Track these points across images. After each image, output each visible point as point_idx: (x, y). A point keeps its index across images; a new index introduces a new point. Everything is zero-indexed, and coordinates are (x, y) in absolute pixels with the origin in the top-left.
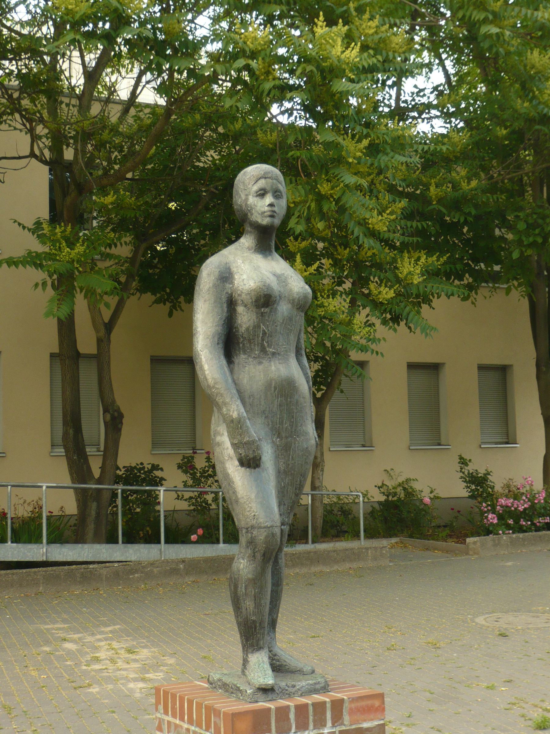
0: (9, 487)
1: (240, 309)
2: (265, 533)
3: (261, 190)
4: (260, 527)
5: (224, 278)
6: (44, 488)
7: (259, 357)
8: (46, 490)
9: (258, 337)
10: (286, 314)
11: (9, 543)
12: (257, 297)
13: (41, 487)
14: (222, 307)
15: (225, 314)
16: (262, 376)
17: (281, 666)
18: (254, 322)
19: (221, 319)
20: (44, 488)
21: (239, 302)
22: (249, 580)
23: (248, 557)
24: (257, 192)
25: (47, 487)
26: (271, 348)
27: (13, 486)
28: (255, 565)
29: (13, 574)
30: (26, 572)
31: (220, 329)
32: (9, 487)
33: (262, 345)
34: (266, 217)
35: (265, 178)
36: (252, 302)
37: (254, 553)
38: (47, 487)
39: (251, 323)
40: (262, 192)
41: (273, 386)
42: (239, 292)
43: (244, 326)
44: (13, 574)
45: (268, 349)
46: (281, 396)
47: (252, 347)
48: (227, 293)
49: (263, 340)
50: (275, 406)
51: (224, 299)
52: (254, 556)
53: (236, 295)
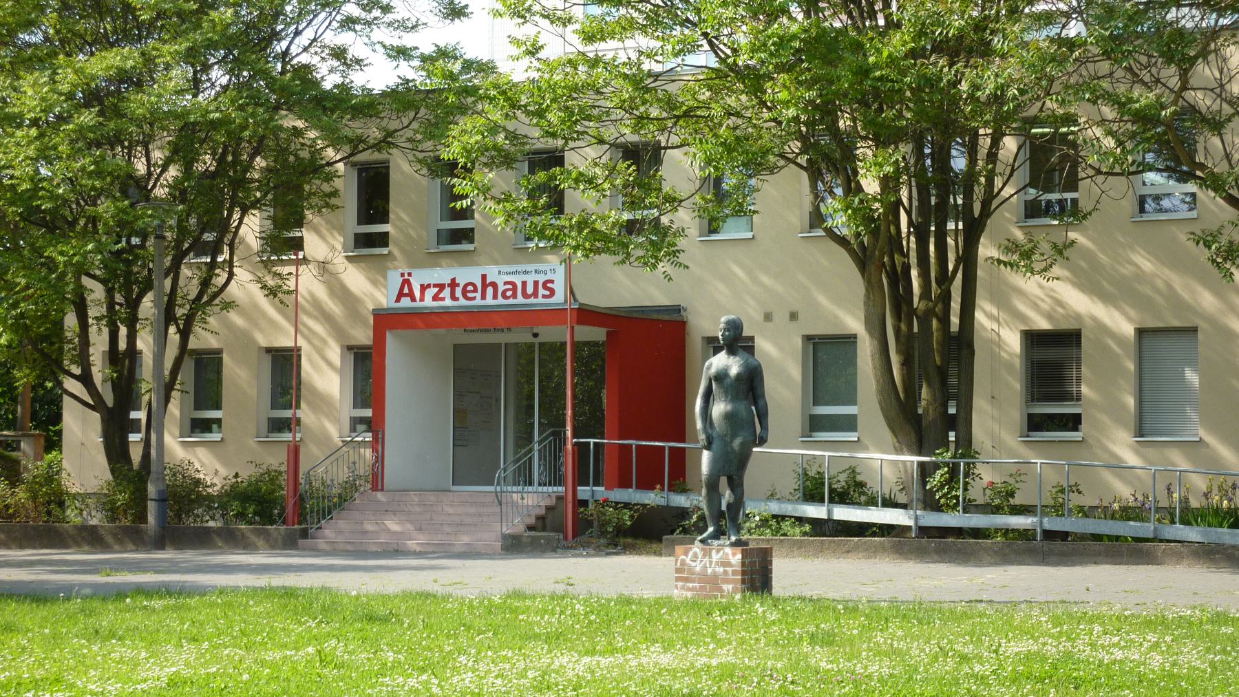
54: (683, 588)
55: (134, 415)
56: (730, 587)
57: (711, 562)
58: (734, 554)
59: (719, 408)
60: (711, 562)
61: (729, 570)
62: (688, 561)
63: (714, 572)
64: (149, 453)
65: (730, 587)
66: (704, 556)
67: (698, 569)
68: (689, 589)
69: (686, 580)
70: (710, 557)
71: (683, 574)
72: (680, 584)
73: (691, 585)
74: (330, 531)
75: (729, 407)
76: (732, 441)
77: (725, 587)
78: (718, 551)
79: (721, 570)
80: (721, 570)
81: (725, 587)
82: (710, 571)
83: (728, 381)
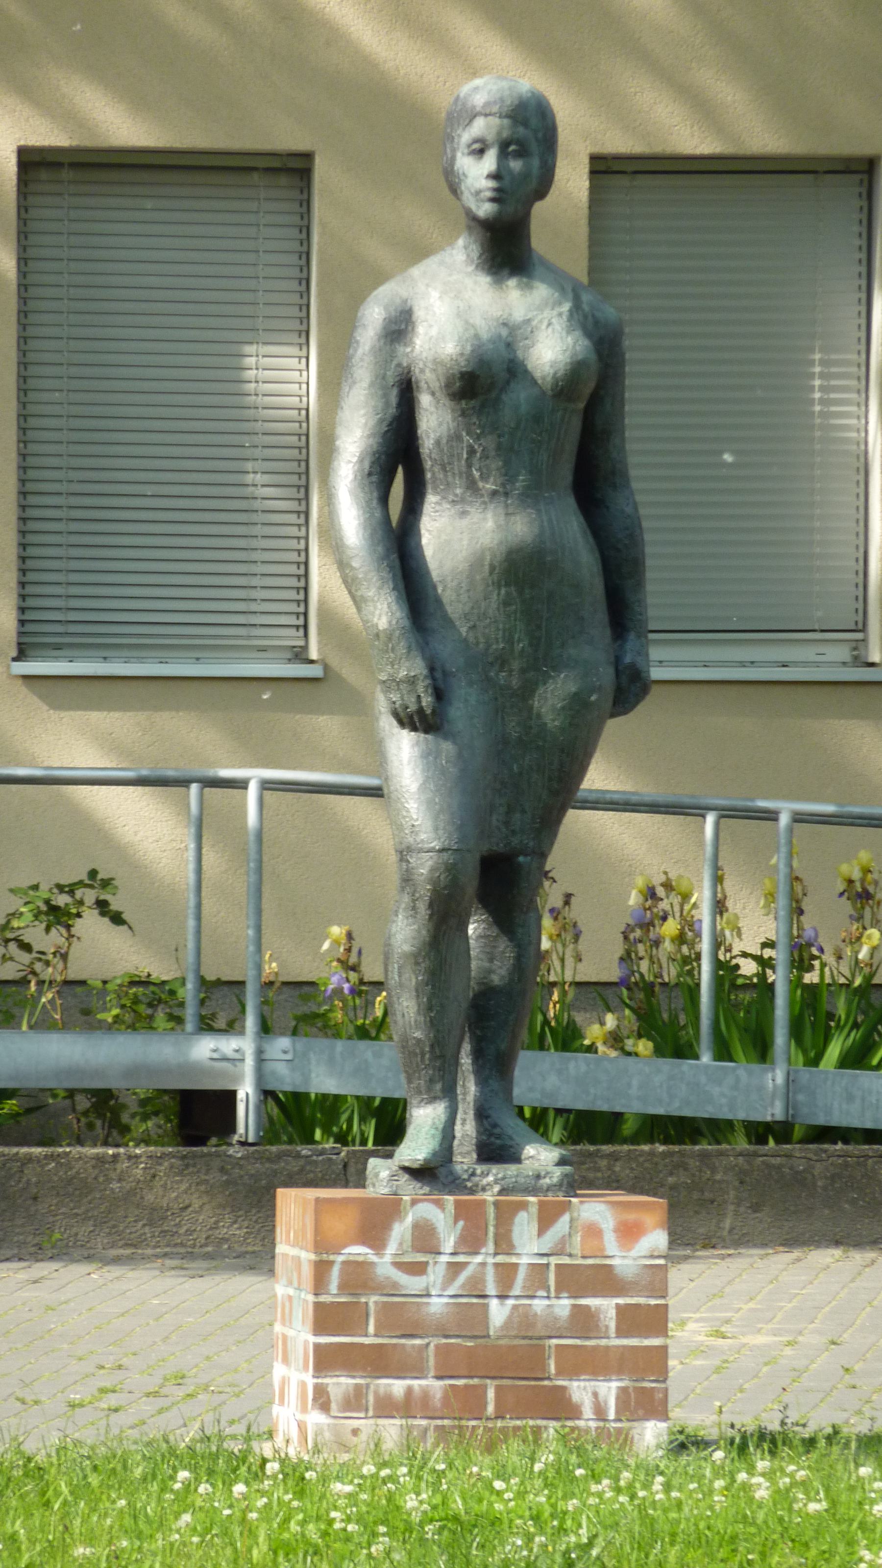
0: (710, 819)
1: (425, 400)
2: (430, 863)
3: (476, 141)
4: (421, 851)
5: (394, 332)
6: (784, 819)
7: (463, 501)
8: (790, 830)
9: (459, 460)
10: (524, 409)
11: (706, 1058)
12: (448, 378)
13: (772, 816)
14: (385, 396)
15: (392, 411)
16: (465, 542)
17: (503, 1147)
18: (449, 429)
19: (381, 421)
20: (784, 819)
21: (423, 385)
22: (405, 955)
23: (405, 909)
24: (469, 146)
25: (799, 818)
26: (487, 482)
27: (727, 813)
28: (415, 927)
29: (614, 1157)
30: (664, 1155)
31: (374, 442)
32: (710, 819)
33: (469, 475)
34: (483, 201)
35: (486, 115)
36: (440, 387)
37: (414, 901)
38: (799, 818)
39: (443, 431)
40: (476, 146)
41: (487, 563)
42: (421, 365)
43: (432, 436)
44: (614, 1157)
45: (481, 484)
46: (507, 585)
47: (450, 479)
48: (399, 365)
49: (469, 466)
50: (494, 605)
51: (391, 376)
52: (414, 908)
53: (417, 371)
54: (354, 1402)
55: (771, 1143)
56: (610, 1390)
57: (507, 1273)
58: (629, 1233)
59: (457, 534)
60: (507, 1273)
61: (606, 1307)
62: (384, 1264)
63: (523, 1321)
64: (720, 1030)
65: (610, 1390)
66: (471, 1242)
67: (437, 1304)
68: (386, 1408)
69: (378, 1362)
70: (504, 1244)
71: (357, 1339)
72: (340, 1384)
73: (397, 1387)
74: (442, 686)
75: (522, 527)
76: (527, 691)
77: (580, 1390)
78: (546, 1220)
79: (563, 1306)
80: (563, 1306)
81: (580, 1390)
82: (498, 1313)
83: (519, 398)
